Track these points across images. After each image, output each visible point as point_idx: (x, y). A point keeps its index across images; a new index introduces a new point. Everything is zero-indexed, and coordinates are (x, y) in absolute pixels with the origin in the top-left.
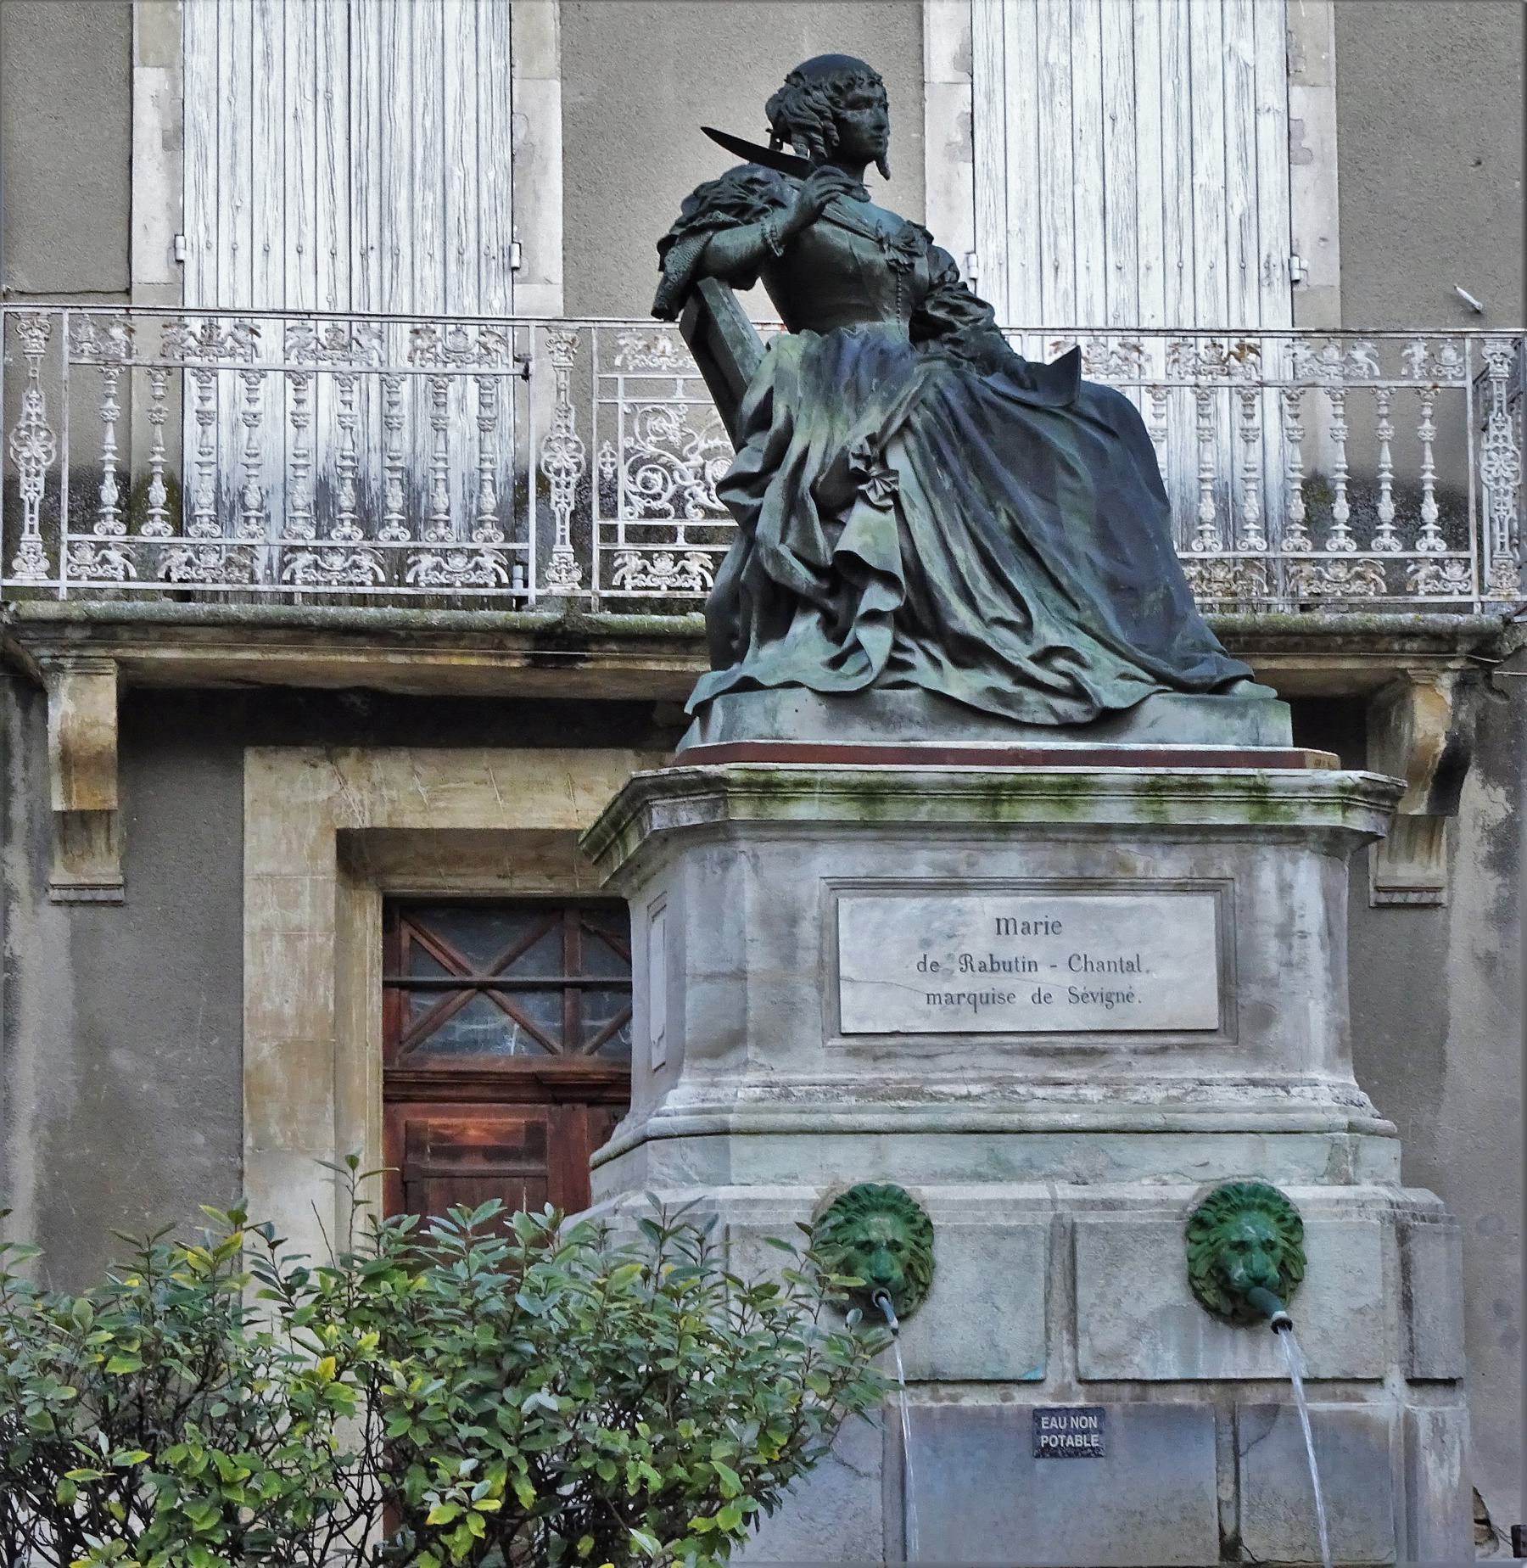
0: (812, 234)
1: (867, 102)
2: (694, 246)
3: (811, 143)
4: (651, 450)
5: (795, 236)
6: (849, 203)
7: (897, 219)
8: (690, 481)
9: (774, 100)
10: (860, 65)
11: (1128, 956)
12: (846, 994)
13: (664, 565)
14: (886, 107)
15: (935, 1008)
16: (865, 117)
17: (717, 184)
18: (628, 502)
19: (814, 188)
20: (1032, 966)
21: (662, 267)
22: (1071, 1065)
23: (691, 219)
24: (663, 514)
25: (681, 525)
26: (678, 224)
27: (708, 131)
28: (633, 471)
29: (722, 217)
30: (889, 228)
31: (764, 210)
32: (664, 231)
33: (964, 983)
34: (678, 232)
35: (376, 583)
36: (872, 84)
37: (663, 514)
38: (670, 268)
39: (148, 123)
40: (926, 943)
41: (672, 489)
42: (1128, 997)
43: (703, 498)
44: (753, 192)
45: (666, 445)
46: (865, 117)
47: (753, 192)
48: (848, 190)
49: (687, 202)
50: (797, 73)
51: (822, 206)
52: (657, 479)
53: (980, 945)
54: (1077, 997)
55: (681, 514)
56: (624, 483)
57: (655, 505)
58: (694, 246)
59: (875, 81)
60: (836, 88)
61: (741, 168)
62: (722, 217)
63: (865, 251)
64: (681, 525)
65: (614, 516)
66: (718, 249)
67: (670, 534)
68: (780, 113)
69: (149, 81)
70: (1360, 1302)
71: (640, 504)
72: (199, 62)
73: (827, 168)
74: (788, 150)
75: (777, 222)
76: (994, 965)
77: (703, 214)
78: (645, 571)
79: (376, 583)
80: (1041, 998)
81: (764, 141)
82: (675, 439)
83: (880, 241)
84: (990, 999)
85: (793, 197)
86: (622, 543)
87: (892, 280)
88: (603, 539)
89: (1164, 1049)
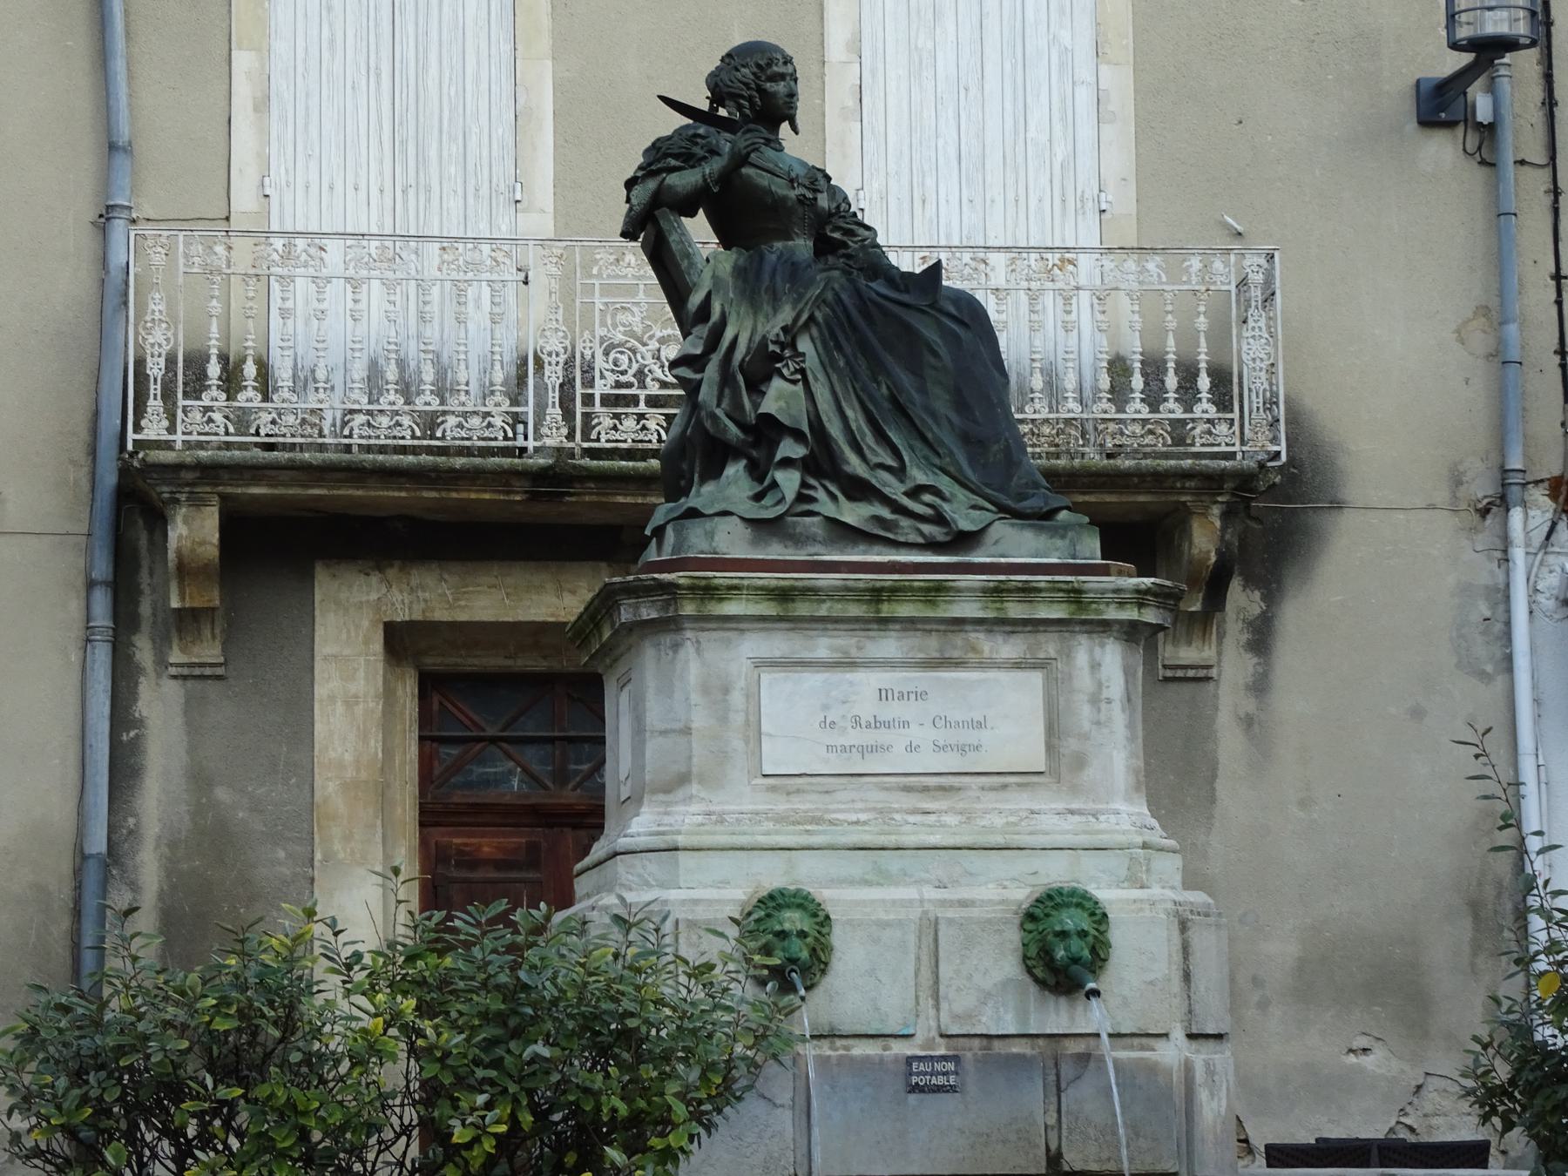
0: (741, 176)
1: (782, 77)
2: (652, 185)
3: (740, 108)
4: (620, 337)
5: (728, 177)
6: (769, 152)
7: (804, 164)
8: (649, 361)
9: (712, 75)
10: (777, 49)
11: (978, 717)
13: (630, 424)
14: (796, 80)
15: (832, 756)
16: (781, 88)
17: (669, 138)
18: (602, 377)
19: (742, 141)
21: (628, 200)
23: (650, 164)
24: (629, 385)
25: (642, 394)
26: (640, 168)
27: (662, 98)
28: (606, 354)
29: (673, 162)
30: (798, 171)
31: (705, 158)
32: (630, 174)
33: (854, 737)
34: (640, 174)
35: (413, 437)
36: (785, 63)
37: (629, 385)
38: (634, 201)
40: (826, 707)
41: (635, 366)
43: (659, 373)
44: (696, 144)
45: (632, 334)
46: (781, 88)
47: (696, 144)
48: (768, 142)
49: (647, 151)
50: (729, 55)
51: (748, 154)
52: (624, 359)
53: (867, 707)
54: (938, 748)
55: (643, 386)
56: (600, 363)
57: (623, 379)
58: (652, 185)
59: (788, 61)
60: (758, 66)
61: (687, 126)
62: (673, 162)
63: (780, 188)
64: (642, 394)
65: (592, 387)
66: (670, 187)
67: (634, 400)
68: (716, 85)
69: (242, 61)
70: (1151, 977)
71: (611, 378)
72: (280, 47)
73: (752, 126)
74: (722, 112)
75: (714, 166)
76: (877, 724)
77: (658, 161)
78: (615, 428)
79: (413, 437)
80: (912, 748)
81: (704, 105)
82: (638, 329)
83: (792, 181)
84: (874, 749)
85: (727, 147)
86: (598, 408)
87: (800, 210)
88: (592, 395)
89: (1005, 787)
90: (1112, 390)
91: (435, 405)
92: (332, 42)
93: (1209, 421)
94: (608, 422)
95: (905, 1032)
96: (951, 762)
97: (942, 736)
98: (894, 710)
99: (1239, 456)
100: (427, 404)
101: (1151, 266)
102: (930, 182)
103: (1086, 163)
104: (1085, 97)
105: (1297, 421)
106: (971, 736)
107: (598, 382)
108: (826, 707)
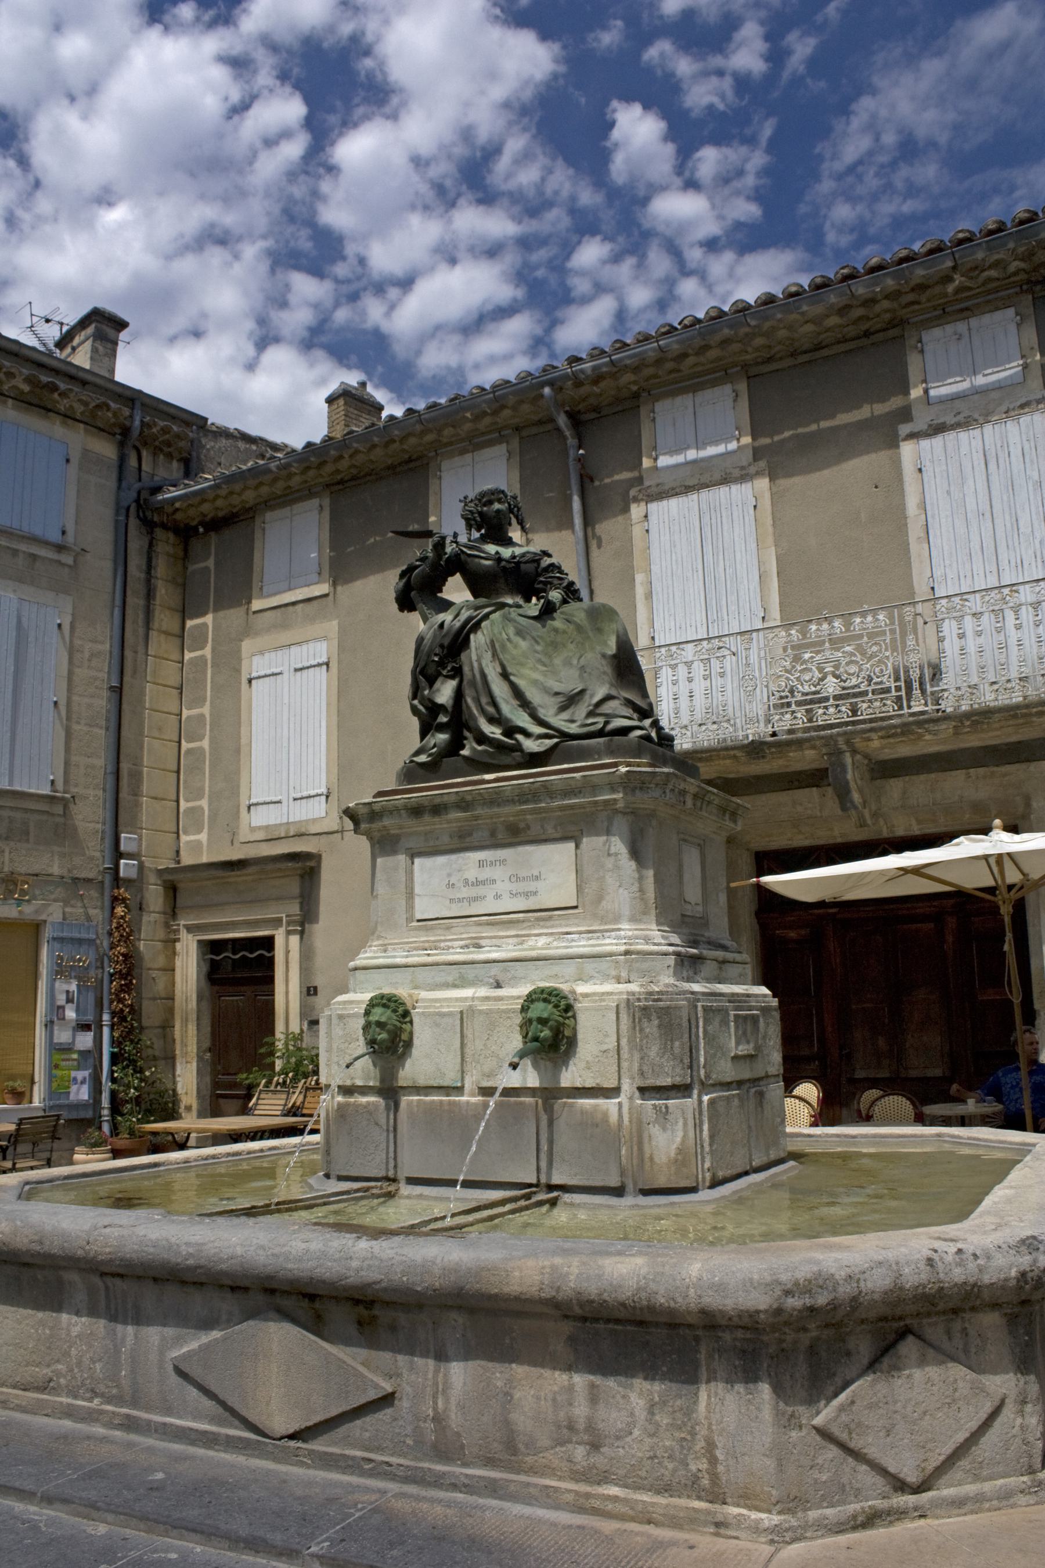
11: (536, 873)
12: (417, 901)
15: (453, 905)
20: (494, 881)
22: (508, 929)
33: (465, 892)
39: (640, 591)
40: (449, 875)
42: (535, 893)
53: (472, 874)
54: (513, 895)
55: (793, 696)
69: (639, 578)
70: (605, 1047)
72: (654, 568)
76: (478, 883)
80: (497, 897)
84: (476, 899)
86: (772, 711)
89: (550, 918)
96: (521, 904)
97: (515, 887)
98: (487, 873)
106: (532, 886)
108: (449, 875)
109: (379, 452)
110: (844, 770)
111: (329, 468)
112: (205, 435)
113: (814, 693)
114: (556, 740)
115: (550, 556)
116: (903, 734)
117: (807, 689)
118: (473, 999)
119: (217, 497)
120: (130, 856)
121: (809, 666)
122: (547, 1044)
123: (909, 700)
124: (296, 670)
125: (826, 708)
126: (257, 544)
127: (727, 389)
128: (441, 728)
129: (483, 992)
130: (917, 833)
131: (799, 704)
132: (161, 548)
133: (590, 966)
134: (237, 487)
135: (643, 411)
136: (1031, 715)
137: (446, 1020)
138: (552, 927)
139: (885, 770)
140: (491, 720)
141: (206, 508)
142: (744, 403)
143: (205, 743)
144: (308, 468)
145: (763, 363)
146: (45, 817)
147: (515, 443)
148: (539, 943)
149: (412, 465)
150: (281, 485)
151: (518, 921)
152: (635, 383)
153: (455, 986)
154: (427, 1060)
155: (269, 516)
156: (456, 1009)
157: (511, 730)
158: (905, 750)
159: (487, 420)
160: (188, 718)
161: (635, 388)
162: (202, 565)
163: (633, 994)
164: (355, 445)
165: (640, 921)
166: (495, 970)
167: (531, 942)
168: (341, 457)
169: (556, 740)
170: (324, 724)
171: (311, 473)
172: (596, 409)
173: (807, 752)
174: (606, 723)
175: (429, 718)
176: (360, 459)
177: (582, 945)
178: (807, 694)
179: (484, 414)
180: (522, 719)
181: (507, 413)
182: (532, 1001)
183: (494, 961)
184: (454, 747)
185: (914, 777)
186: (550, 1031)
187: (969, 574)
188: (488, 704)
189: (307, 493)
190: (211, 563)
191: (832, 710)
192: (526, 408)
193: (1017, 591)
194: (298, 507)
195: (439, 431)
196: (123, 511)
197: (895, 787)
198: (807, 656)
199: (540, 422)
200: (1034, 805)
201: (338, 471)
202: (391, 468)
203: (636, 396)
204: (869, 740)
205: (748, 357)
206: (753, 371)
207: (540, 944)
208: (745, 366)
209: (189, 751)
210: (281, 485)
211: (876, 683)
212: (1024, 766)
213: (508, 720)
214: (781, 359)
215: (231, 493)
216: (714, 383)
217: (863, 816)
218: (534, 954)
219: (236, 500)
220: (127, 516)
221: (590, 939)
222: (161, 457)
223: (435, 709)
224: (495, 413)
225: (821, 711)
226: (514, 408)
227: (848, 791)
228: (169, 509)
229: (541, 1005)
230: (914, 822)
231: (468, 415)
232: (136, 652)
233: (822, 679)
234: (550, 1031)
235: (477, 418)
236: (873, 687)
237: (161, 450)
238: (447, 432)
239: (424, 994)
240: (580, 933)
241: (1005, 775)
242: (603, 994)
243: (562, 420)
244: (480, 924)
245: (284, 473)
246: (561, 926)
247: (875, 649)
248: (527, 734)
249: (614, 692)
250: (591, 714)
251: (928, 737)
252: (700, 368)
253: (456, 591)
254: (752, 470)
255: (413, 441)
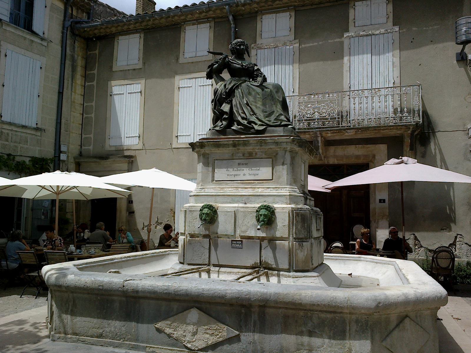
15: (228, 177)
55: (304, 118)
78: (299, 125)
80: (244, 175)
86: (297, 122)
89: (263, 183)
90: (401, 111)
91: (401, 115)
92: (266, 70)
93: (406, 116)
94: (298, 124)
95: (233, 215)
99: (412, 122)
100: (399, 115)
101: (335, 95)
102: (362, 81)
103: (391, 74)
104: (391, 64)
105: (425, 114)
107: (297, 118)
109: (163, 20)
110: (318, 142)
111: (144, 24)
112: (96, 5)
113: (311, 117)
114: (265, 127)
115: (257, 66)
116: (338, 132)
117: (308, 116)
118: (238, 207)
119: (101, 28)
120: (64, 153)
121: (310, 109)
122: (266, 222)
123: (342, 122)
124: (129, 93)
125: (314, 122)
126: (115, 47)
127: (288, 13)
128: (225, 119)
129: (241, 205)
130: (337, 163)
131: (305, 120)
132: (77, 44)
133: (277, 199)
134: (109, 26)
135: (258, 18)
136: (381, 130)
137: (229, 213)
138: (263, 185)
139: (329, 143)
140: (243, 118)
141: (96, 31)
142: (293, 19)
143: (93, 115)
144: (137, 23)
145: (300, 6)
146: (34, 136)
147: (213, 24)
148: (259, 191)
149: (175, 26)
150: (126, 27)
151: (252, 183)
152: (257, 8)
153: (230, 203)
154: (224, 225)
155: (120, 38)
156: (233, 210)
157: (250, 122)
158: (337, 137)
159: (204, 14)
160: (86, 106)
161: (257, 10)
162: (94, 52)
163: (293, 208)
164: (156, 16)
165: (292, 185)
166: (245, 198)
167: (257, 190)
168: (150, 20)
169: (265, 127)
170: (138, 113)
171: (137, 25)
172: (242, 15)
173: (307, 136)
174: (281, 123)
175: (218, 116)
176: (157, 22)
177: (274, 192)
178: (308, 118)
179: (203, 12)
180: (253, 119)
181: (211, 12)
182: (261, 209)
183: (244, 195)
184: (229, 125)
185: (338, 146)
186: (267, 218)
187: (362, 84)
188: (242, 113)
189: (135, 31)
190: (97, 52)
191: (316, 123)
192: (218, 11)
193: (380, 91)
194: (132, 36)
195: (187, 16)
196: (66, 29)
197: (332, 149)
198: (309, 106)
199: (222, 17)
200: (376, 157)
201: (148, 25)
202: (167, 26)
203: (257, 12)
204: (327, 133)
205: (296, 4)
206: (297, 9)
207: (259, 191)
208: (295, 6)
209: (86, 118)
210: (126, 27)
211: (331, 116)
212: (374, 145)
213: (249, 119)
214: (307, 6)
215: (107, 28)
216: (284, 11)
217: (321, 157)
218: (258, 194)
219: (108, 30)
220: (67, 31)
221: (276, 190)
222: (80, 11)
223: (223, 113)
224: (207, 12)
225: (312, 123)
226: (214, 11)
227: (319, 149)
228: (81, 30)
229: (264, 210)
230: (336, 160)
231: (198, 11)
232: (68, 80)
233: (313, 113)
234: (267, 218)
235: (201, 13)
236: (330, 117)
237: (80, 8)
238: (190, 16)
239: (220, 205)
240: (273, 188)
241: (368, 148)
242: (283, 208)
243: (231, 18)
244: (242, 183)
245: (128, 23)
246: (266, 185)
247: (332, 105)
248: (256, 124)
249: (282, 113)
250: (276, 119)
251: (346, 134)
252: (279, 6)
253: (226, 75)
254: (294, 42)
255: (176, 18)
